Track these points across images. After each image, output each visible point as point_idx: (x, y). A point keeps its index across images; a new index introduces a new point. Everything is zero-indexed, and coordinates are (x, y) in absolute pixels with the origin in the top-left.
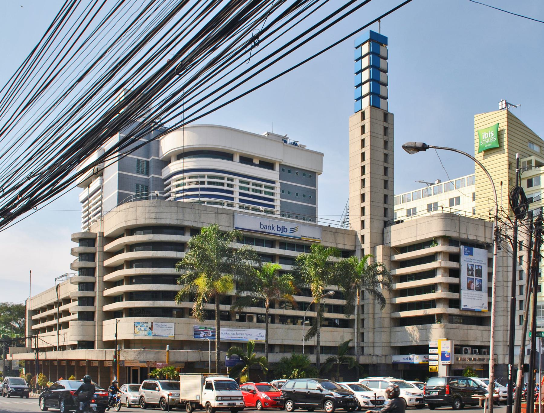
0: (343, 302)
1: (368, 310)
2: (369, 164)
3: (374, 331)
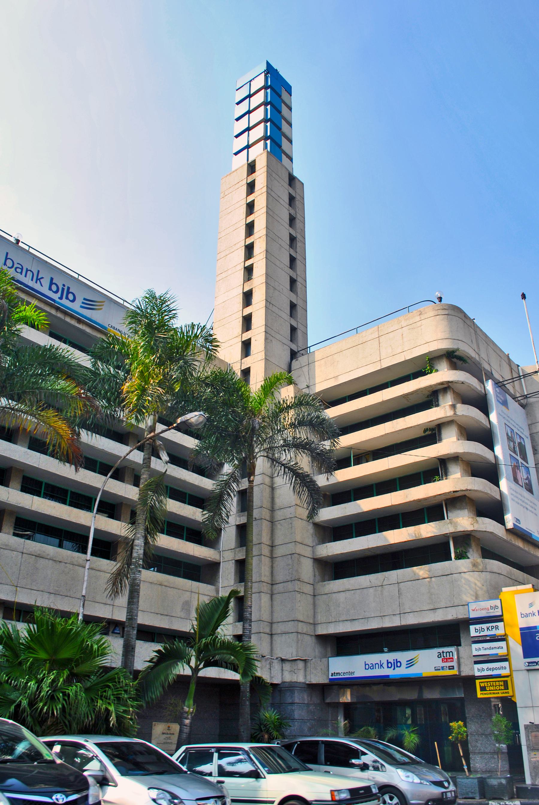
0: (195, 513)
1: (260, 534)
2: (265, 237)
3: (272, 590)
